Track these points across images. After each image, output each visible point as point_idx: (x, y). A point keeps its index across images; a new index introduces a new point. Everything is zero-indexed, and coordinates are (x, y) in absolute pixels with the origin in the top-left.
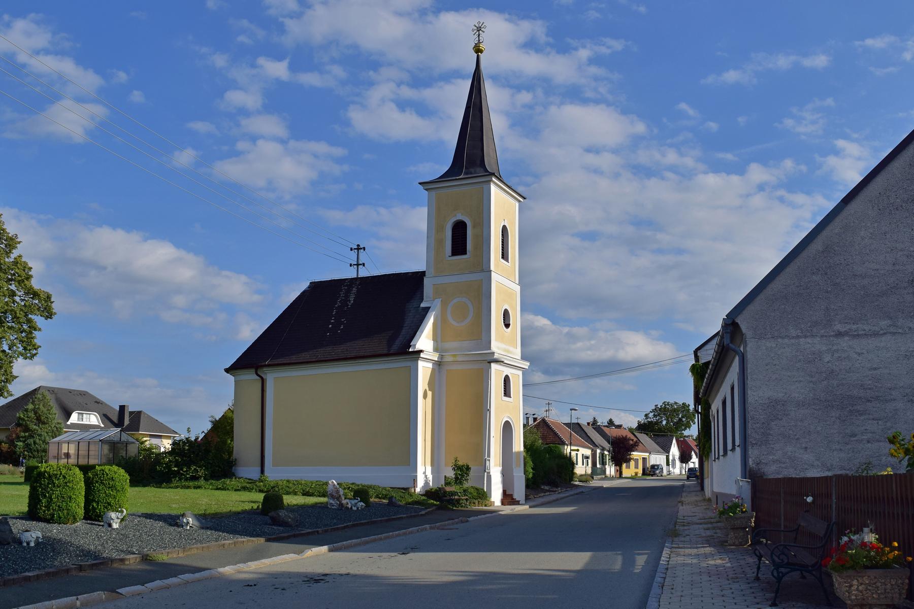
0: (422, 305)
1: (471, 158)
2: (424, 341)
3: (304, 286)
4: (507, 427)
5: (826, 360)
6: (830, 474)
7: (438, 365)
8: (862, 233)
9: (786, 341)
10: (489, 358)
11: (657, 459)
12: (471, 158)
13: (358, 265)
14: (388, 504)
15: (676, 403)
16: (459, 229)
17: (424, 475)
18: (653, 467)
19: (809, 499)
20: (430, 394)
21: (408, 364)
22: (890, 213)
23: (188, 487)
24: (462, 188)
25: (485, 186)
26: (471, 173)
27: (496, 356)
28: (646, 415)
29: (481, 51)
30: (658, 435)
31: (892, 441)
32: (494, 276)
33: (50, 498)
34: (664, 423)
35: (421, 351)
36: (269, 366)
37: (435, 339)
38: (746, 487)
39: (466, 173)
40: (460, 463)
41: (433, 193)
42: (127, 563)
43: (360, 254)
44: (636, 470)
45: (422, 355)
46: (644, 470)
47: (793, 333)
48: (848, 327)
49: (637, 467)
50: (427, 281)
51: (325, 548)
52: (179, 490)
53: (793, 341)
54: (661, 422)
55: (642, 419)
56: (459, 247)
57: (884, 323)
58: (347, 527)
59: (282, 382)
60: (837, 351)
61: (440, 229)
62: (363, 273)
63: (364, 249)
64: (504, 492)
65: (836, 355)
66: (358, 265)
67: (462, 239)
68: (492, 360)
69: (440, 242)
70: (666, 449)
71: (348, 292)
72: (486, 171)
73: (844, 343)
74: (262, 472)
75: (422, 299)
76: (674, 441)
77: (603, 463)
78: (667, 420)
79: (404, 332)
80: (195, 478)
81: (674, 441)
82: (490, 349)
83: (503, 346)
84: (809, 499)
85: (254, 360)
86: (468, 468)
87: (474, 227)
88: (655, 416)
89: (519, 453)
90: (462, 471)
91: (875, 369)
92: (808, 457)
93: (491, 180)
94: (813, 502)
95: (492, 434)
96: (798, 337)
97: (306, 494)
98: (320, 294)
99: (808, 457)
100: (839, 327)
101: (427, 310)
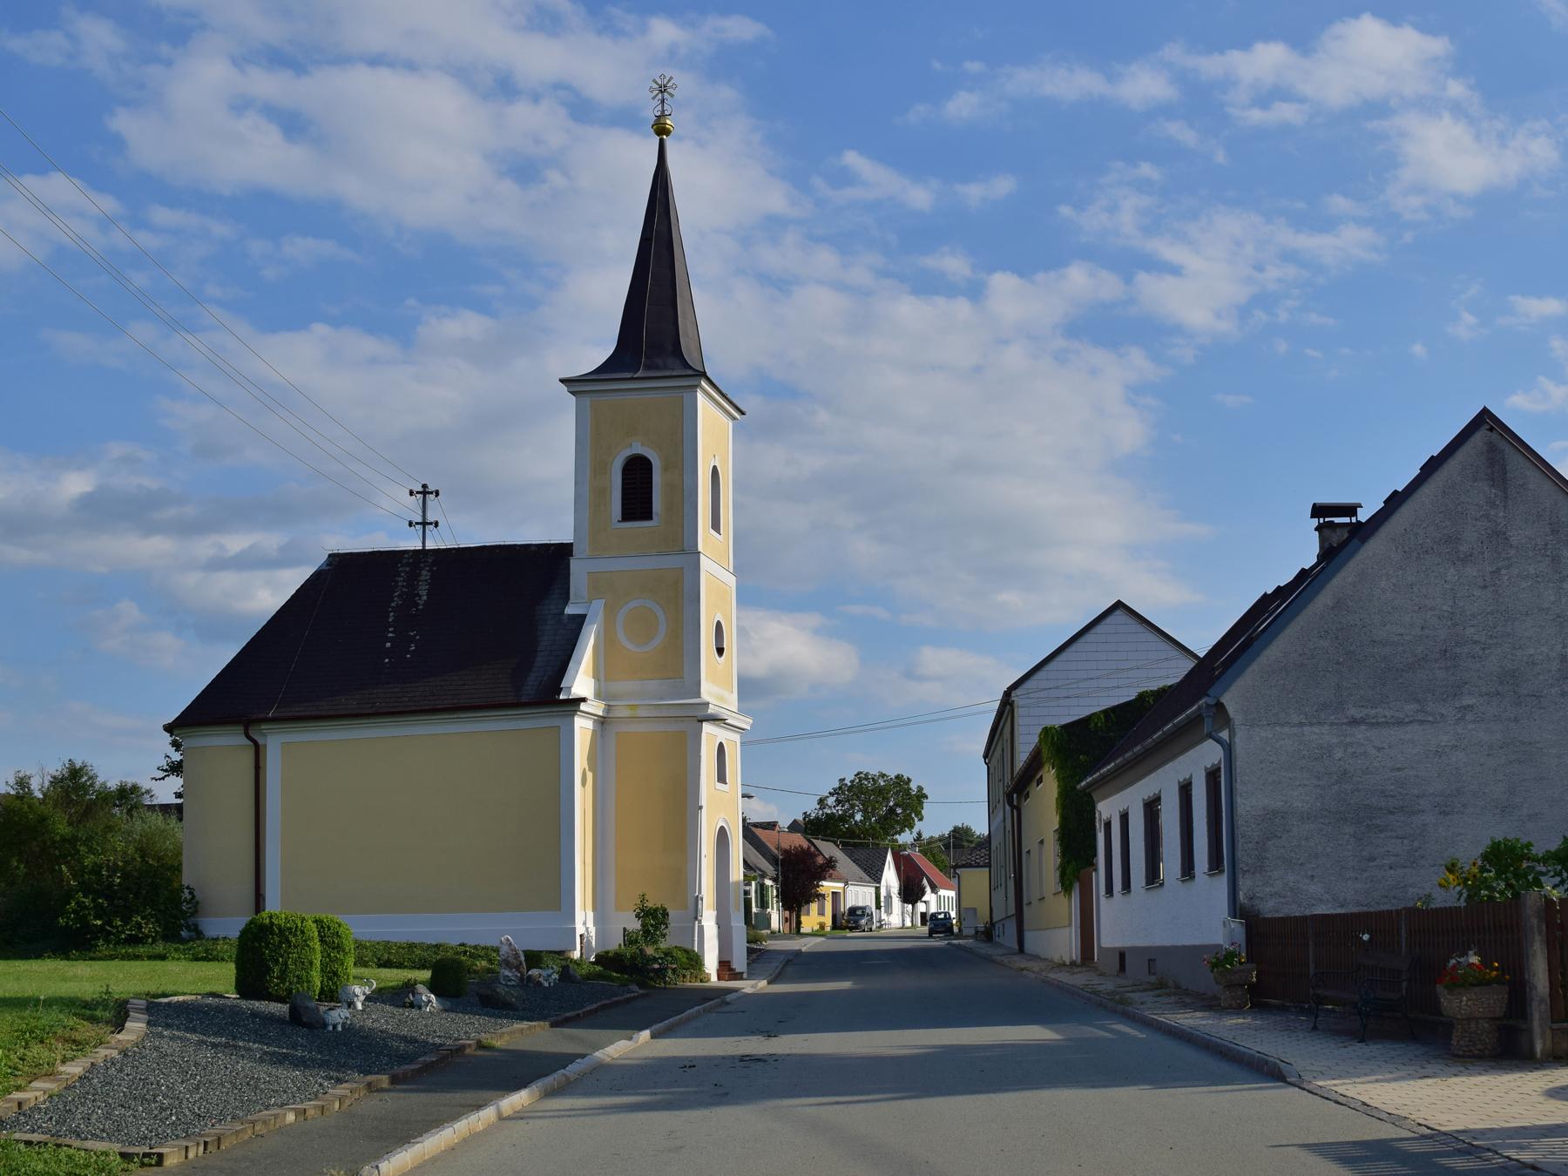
0: (569, 610)
1: (654, 335)
2: (581, 683)
4: (722, 835)
5: (1338, 756)
6: (1342, 911)
7: (602, 722)
8: (1383, 584)
9: (1286, 729)
10: (700, 714)
11: (859, 895)
12: (654, 335)
15: (883, 775)
16: (637, 475)
17: (587, 926)
18: (853, 910)
19: (1366, 937)
20: (590, 775)
21: (556, 722)
22: (1418, 558)
23: (137, 957)
24: (640, 397)
25: (686, 395)
26: (657, 368)
27: (711, 710)
28: (821, 801)
29: (668, 133)
30: (855, 845)
31: (1451, 868)
32: (704, 562)
33: (285, 964)
34: (858, 817)
36: (274, 720)
37: (596, 676)
38: (1237, 926)
39: (648, 368)
40: (650, 905)
41: (587, 400)
42: (468, 1051)
43: (429, 503)
44: (822, 919)
45: (583, 707)
46: (834, 917)
47: (1295, 719)
48: (1366, 711)
49: (821, 913)
50: (576, 566)
51: (646, 1034)
52: (116, 962)
53: (1295, 730)
54: (852, 816)
55: (812, 807)
56: (637, 503)
57: (1411, 708)
60: (1351, 744)
61: (600, 468)
62: (436, 541)
65: (1350, 750)
66: (424, 524)
67: (641, 490)
68: (703, 716)
69: (600, 494)
70: (875, 875)
71: (413, 578)
72: (686, 365)
73: (1360, 733)
75: (565, 598)
76: (889, 857)
77: (763, 904)
78: (865, 811)
80: (134, 940)
81: (889, 857)
82: (698, 695)
84: (1366, 937)
86: (665, 914)
87: (666, 469)
88: (838, 802)
89: (737, 883)
90: (654, 919)
91: (1399, 769)
92: (1315, 888)
93: (699, 385)
94: (1370, 940)
96: (1301, 724)
97: (387, 964)
98: (349, 584)
99: (1315, 888)
100: (1353, 712)
101: (580, 620)
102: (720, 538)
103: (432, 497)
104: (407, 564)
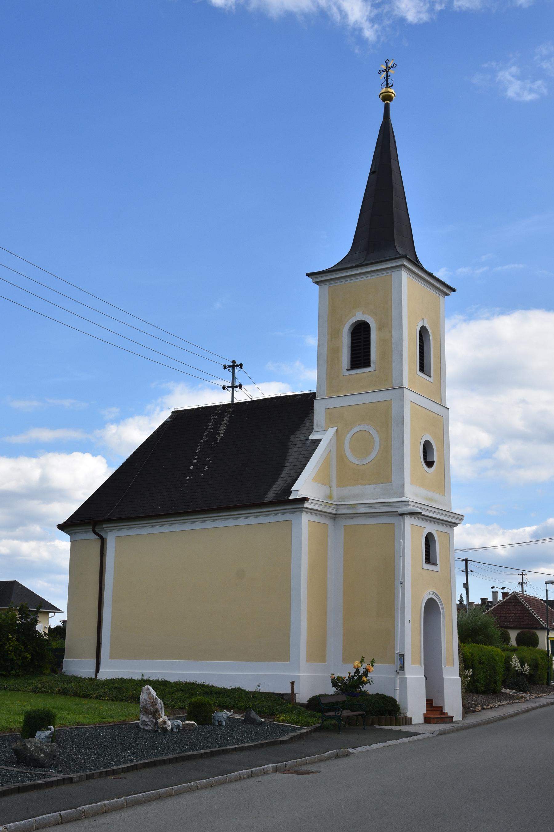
3: (165, 416)
13: (233, 387)
14: (244, 722)
16: (361, 333)
35: (305, 499)
41: (326, 287)
45: (306, 505)
50: (317, 405)
56: (360, 356)
58: (262, 745)
59: (130, 547)
61: (334, 334)
62: (241, 397)
63: (225, 367)
64: (429, 703)
74: (97, 670)
75: (311, 430)
79: (285, 473)
82: (403, 495)
83: (423, 492)
85: (92, 519)
87: (380, 329)
95: (408, 617)
102: (431, 380)
103: (238, 368)
104: (217, 414)
